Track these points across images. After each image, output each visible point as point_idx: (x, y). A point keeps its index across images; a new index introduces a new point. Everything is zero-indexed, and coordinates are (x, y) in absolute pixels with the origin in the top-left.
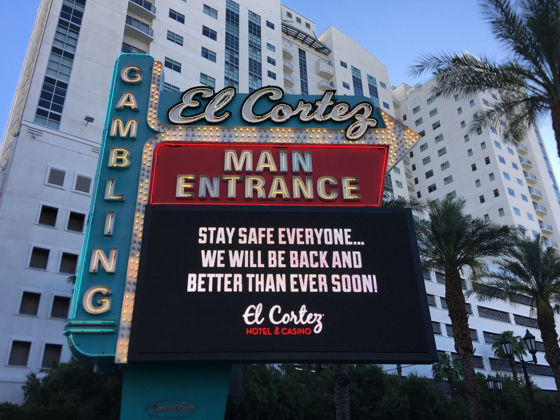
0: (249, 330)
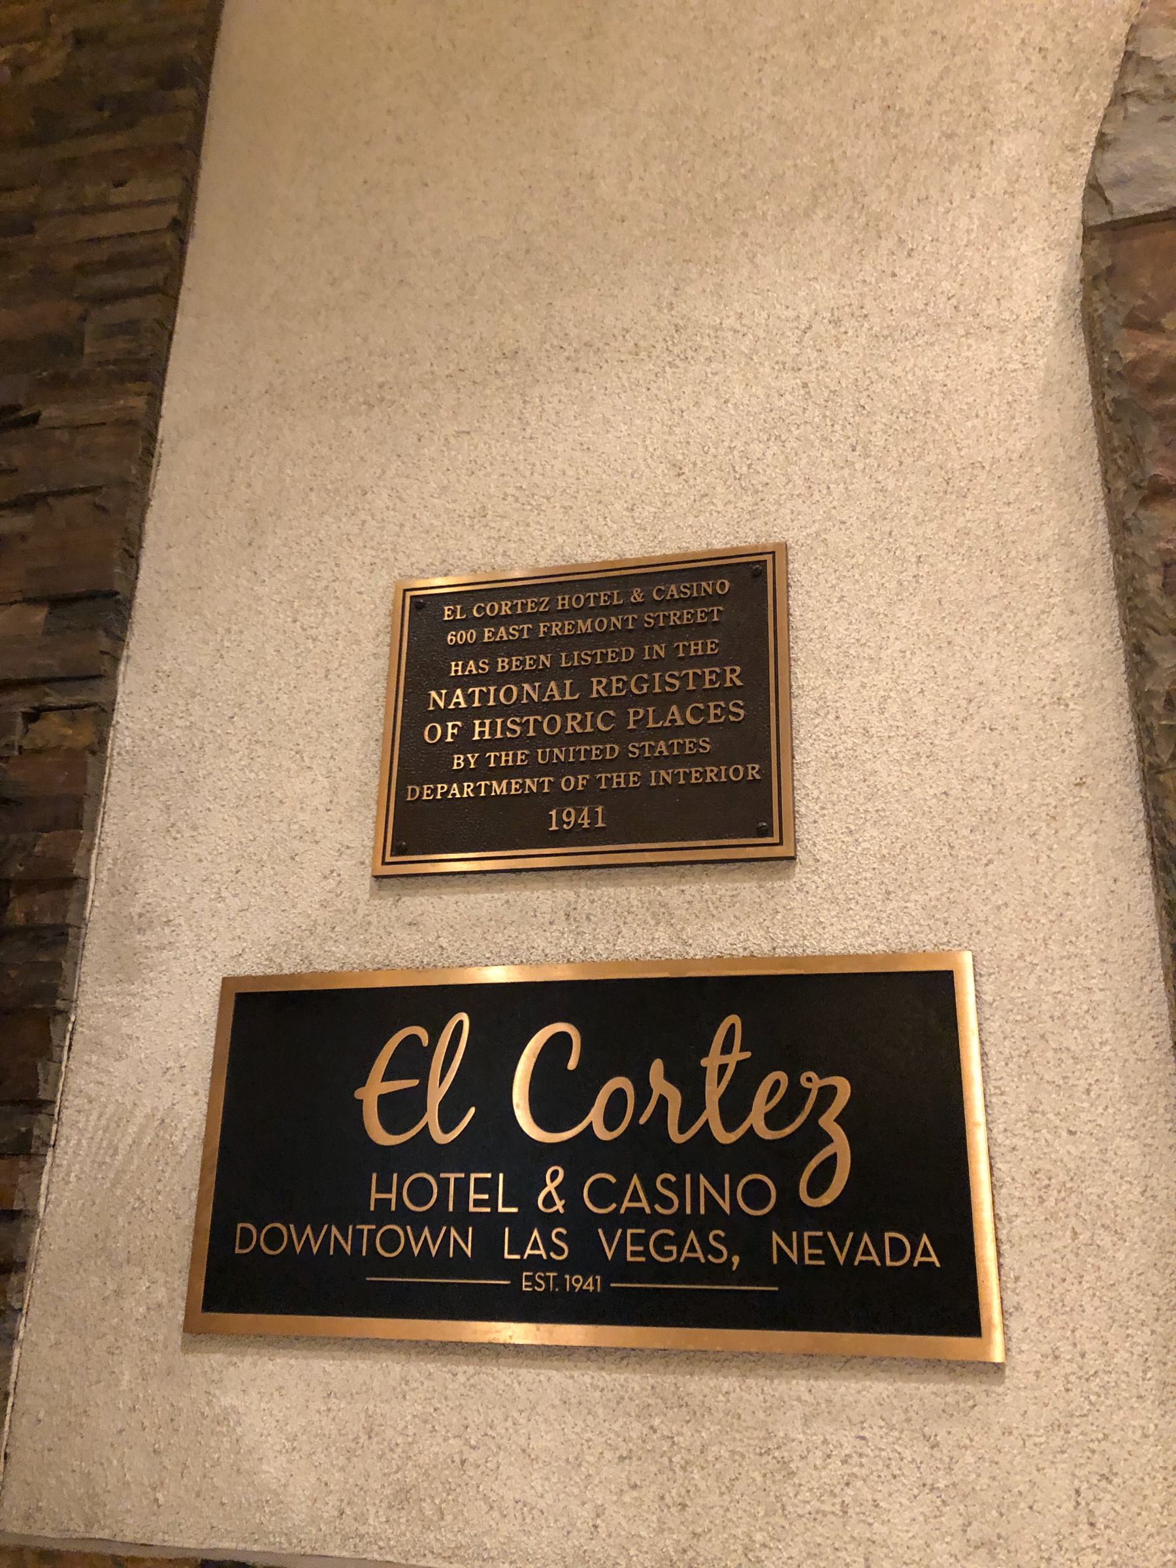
0: (384, 1187)
